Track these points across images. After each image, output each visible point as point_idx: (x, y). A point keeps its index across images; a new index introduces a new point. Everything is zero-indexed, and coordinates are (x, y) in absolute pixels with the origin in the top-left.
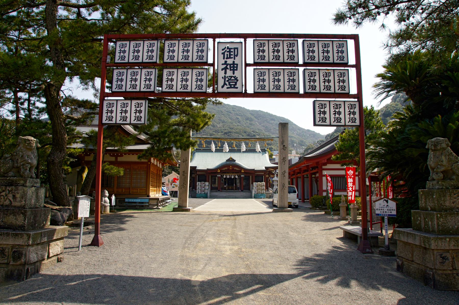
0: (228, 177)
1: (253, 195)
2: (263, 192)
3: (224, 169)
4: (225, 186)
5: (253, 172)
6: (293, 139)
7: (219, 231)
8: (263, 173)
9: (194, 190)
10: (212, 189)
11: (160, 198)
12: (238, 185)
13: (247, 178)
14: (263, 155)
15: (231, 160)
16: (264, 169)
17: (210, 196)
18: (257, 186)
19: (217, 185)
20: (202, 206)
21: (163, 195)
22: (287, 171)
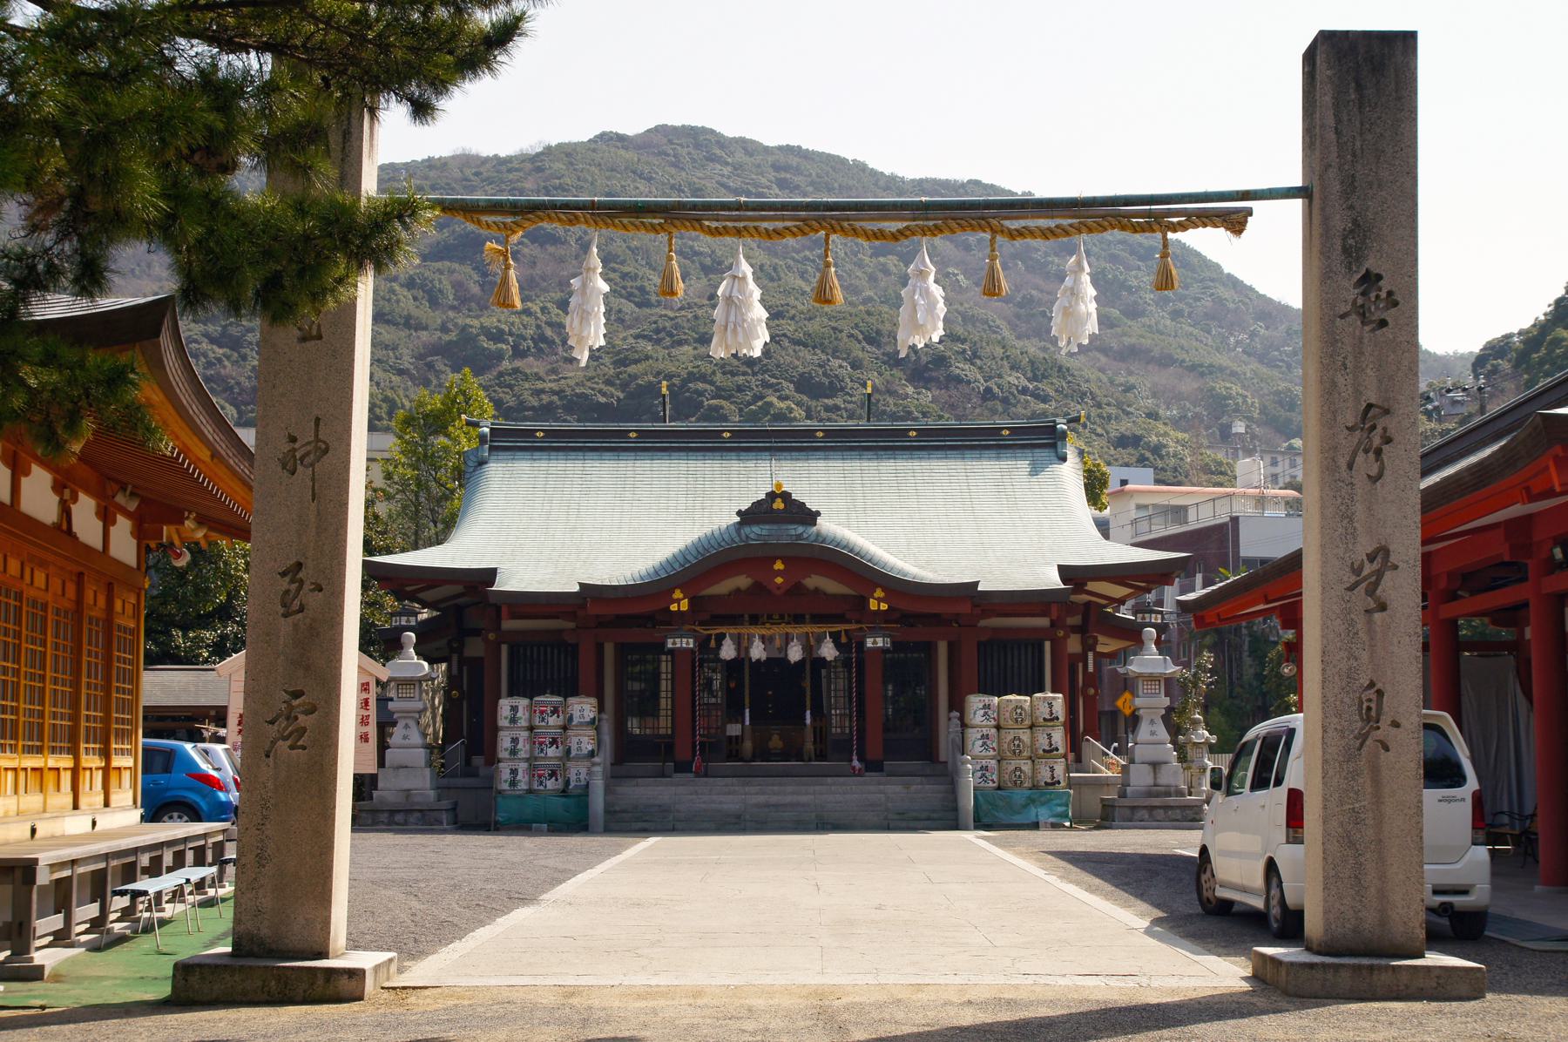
0: (757, 652)
1: (968, 801)
2: (1045, 775)
3: (724, 587)
4: (734, 730)
5: (963, 602)
6: (1220, 386)
7: (834, 329)
8: (1043, 622)
9: (478, 760)
10: (630, 754)
11: (45, 858)
12: (839, 721)
13: (908, 668)
14: (1034, 472)
15: (782, 511)
16: (1054, 581)
17: (609, 810)
18: (995, 727)
19: (664, 724)
20: (521, 914)
21: (155, 810)
22: (1408, 548)
